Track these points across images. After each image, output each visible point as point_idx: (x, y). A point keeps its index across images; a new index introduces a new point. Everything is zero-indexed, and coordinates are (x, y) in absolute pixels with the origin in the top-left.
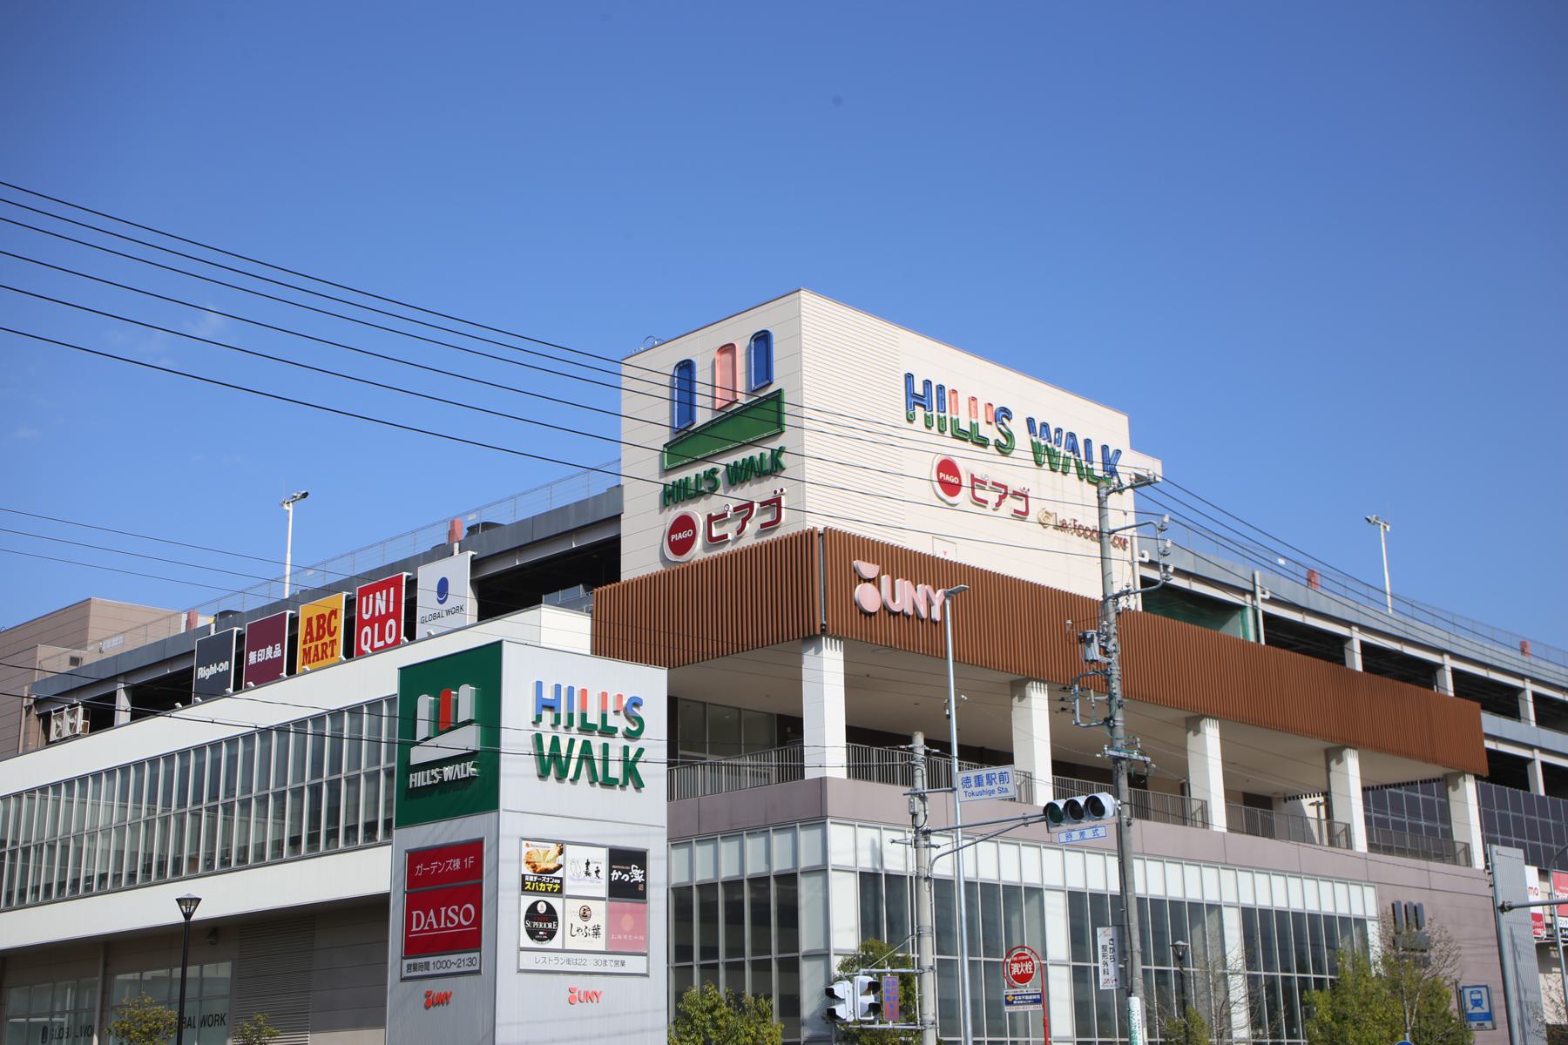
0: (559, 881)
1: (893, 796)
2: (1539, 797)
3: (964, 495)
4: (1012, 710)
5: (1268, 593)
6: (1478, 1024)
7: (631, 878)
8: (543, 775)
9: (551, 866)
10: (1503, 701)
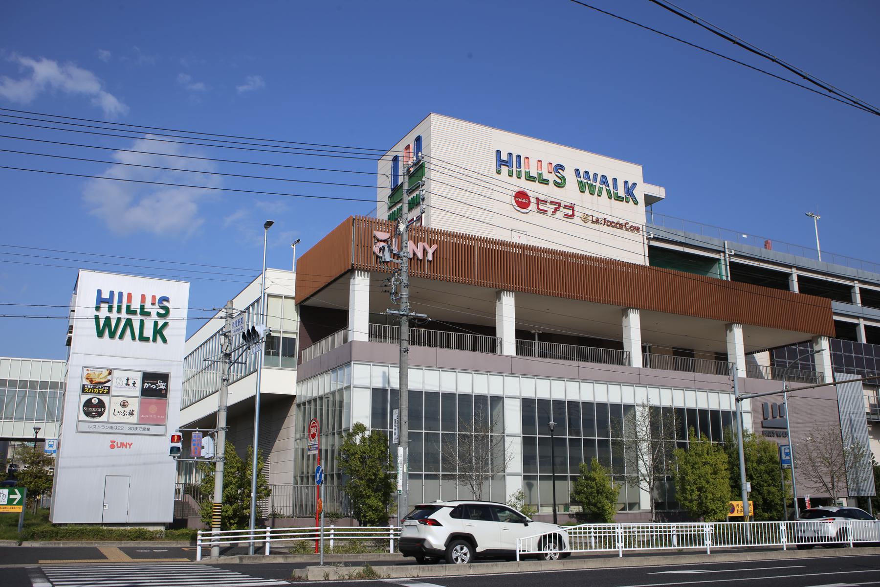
0: (107, 388)
1: (391, 349)
2: (864, 344)
3: (533, 206)
4: (496, 306)
5: (733, 251)
6: (788, 466)
7: (157, 387)
8: (100, 334)
9: (103, 380)
10: (844, 294)
